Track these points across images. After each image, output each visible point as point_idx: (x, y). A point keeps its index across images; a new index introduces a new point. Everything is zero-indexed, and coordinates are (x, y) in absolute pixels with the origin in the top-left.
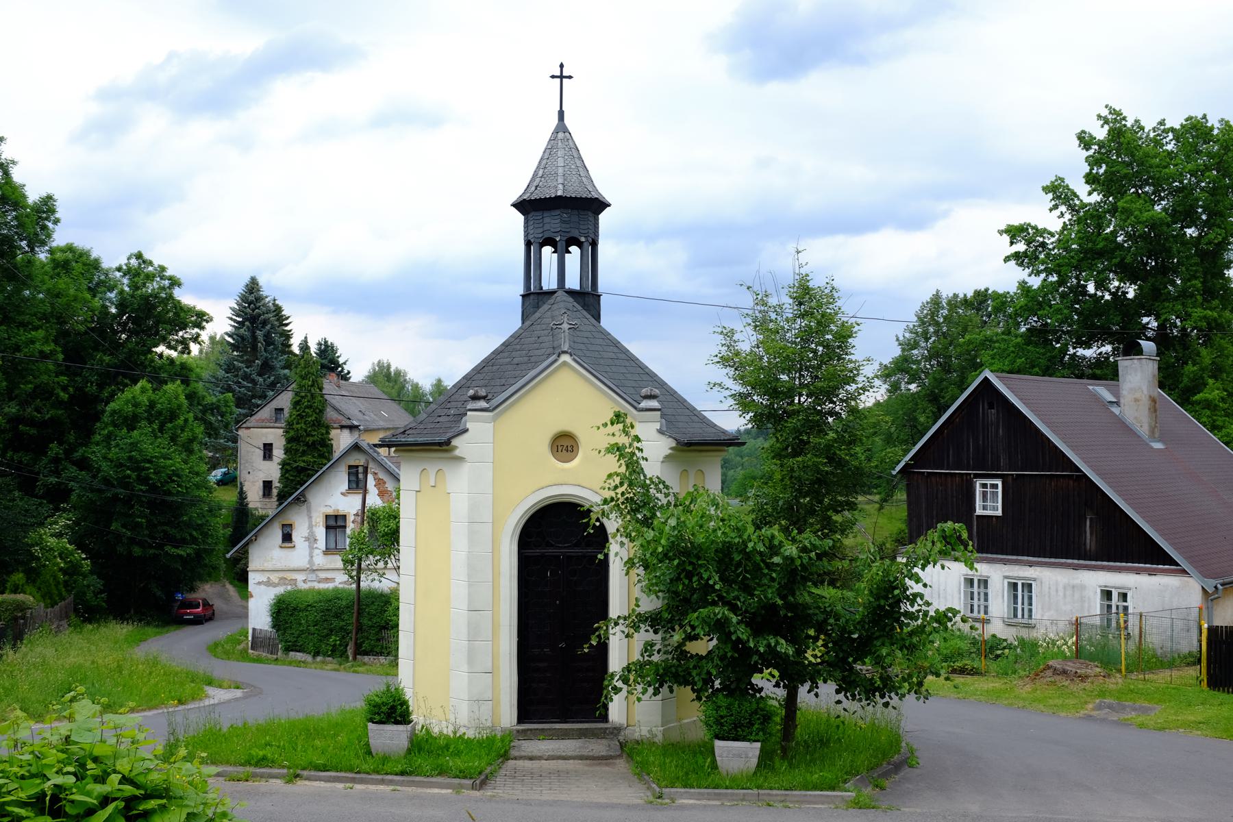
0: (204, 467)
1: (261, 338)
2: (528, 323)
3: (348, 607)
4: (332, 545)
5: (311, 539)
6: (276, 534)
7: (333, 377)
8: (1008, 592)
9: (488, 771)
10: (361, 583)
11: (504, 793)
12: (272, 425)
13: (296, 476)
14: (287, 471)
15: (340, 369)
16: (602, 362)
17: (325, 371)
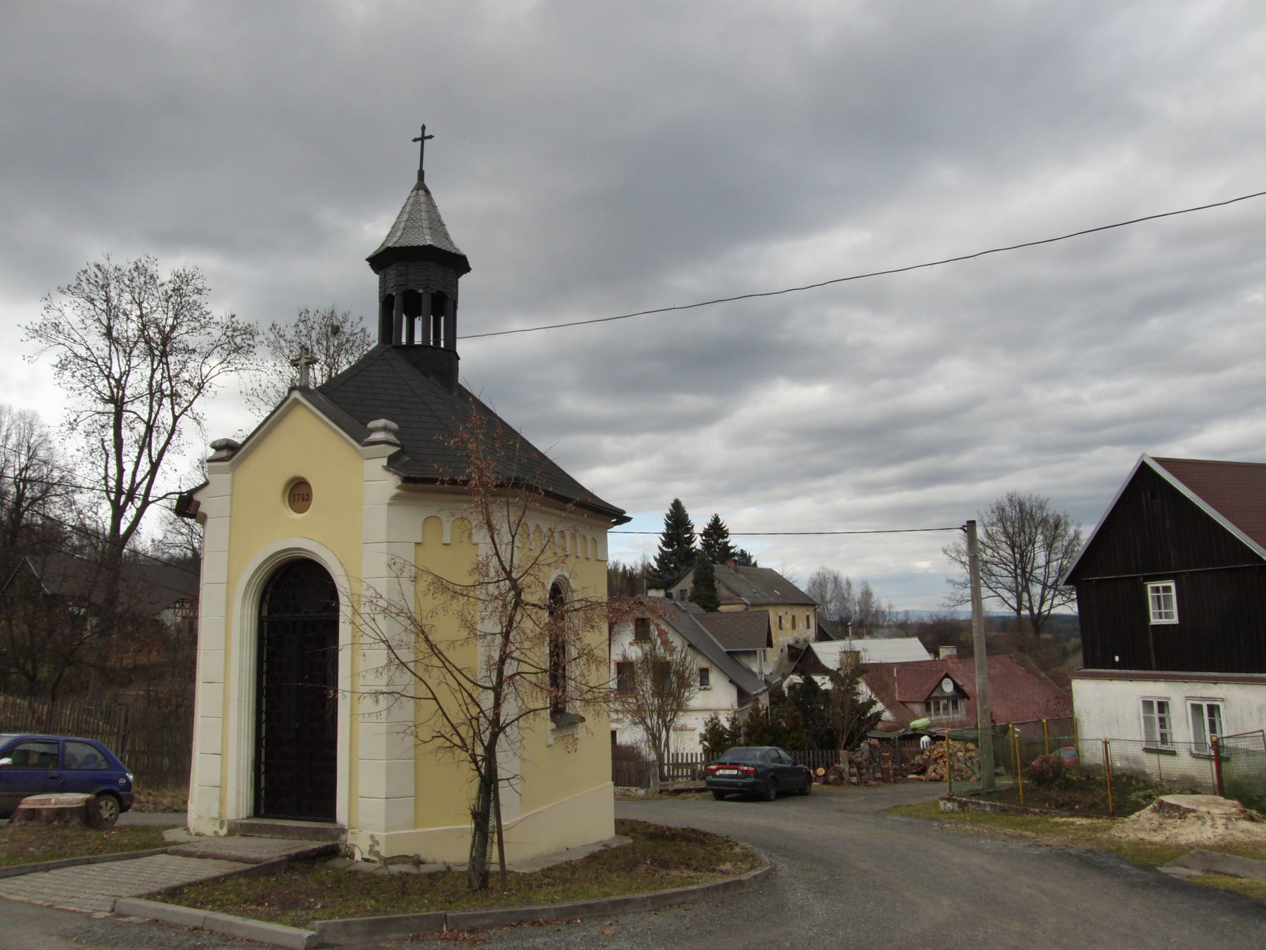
8: (1193, 715)
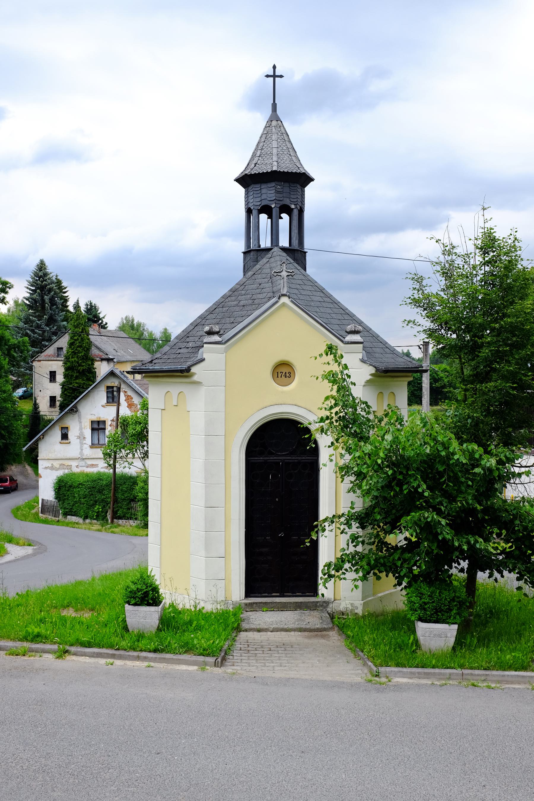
0: (10, 387)
1: (47, 301)
2: (250, 273)
3: (107, 486)
4: (96, 442)
5: (81, 437)
6: (57, 434)
7: (96, 327)
9: (225, 647)
10: (116, 469)
11: (241, 670)
12: (55, 359)
13: (71, 393)
14: (66, 390)
15: (100, 321)
16: (312, 304)
17: (90, 323)
